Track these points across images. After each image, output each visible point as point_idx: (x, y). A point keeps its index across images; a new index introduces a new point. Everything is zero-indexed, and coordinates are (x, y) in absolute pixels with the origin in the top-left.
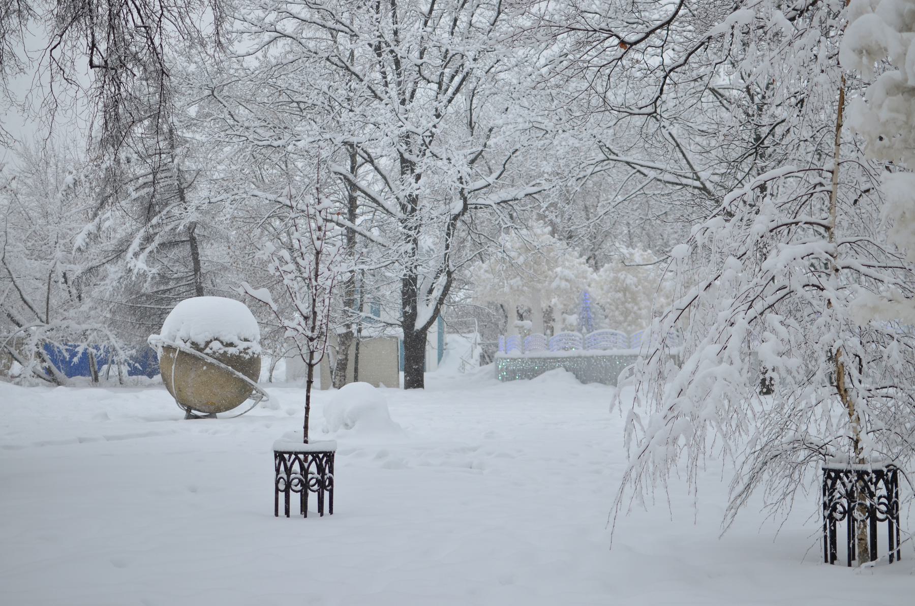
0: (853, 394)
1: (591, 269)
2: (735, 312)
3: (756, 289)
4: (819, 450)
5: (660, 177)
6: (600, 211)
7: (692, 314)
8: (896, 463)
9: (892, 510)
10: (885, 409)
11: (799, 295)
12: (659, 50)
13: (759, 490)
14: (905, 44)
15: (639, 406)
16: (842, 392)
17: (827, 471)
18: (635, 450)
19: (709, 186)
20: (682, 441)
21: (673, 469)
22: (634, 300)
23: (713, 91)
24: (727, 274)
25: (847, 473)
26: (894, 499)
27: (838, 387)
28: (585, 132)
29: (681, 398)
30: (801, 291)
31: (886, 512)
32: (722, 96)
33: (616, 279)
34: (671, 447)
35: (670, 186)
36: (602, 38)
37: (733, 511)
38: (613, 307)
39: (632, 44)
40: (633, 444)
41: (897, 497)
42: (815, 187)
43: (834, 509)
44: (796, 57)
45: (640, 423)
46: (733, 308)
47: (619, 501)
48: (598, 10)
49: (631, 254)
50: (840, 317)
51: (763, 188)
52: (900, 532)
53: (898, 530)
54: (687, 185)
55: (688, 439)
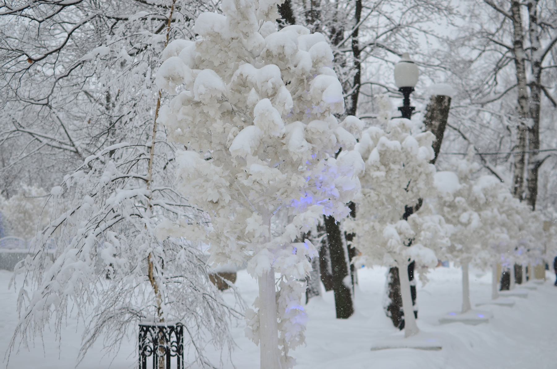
0: (157, 280)
1: (4, 198)
2: (88, 229)
3: (101, 216)
4: (137, 314)
5: (50, 143)
6: (12, 163)
7: (62, 230)
8: (183, 322)
9: (180, 349)
10: (176, 290)
11: (127, 220)
12: (53, 65)
13: (100, 338)
14: (194, 76)
15: (27, 285)
16: (151, 278)
17: (142, 327)
18: (24, 313)
19: (80, 150)
20: (53, 307)
21: (47, 326)
22: (30, 218)
23: (86, 93)
24: (85, 206)
25: (153, 328)
26: (180, 344)
27: (149, 276)
28: (4, 113)
29: (53, 281)
30: (128, 218)
31: (176, 351)
32: (92, 97)
33: (20, 205)
34: (46, 312)
35: (56, 149)
36: (17, 56)
37: (84, 351)
38: (17, 223)
39: (36, 61)
40: (23, 309)
41: (182, 342)
42: (140, 156)
43: (145, 349)
44: (134, 77)
45: (27, 296)
46: (87, 227)
47: (12, 344)
48: (17, 37)
49: (30, 190)
50: (151, 234)
51: (112, 152)
52: (184, 364)
53: (183, 362)
54: (67, 149)
55: (56, 307)
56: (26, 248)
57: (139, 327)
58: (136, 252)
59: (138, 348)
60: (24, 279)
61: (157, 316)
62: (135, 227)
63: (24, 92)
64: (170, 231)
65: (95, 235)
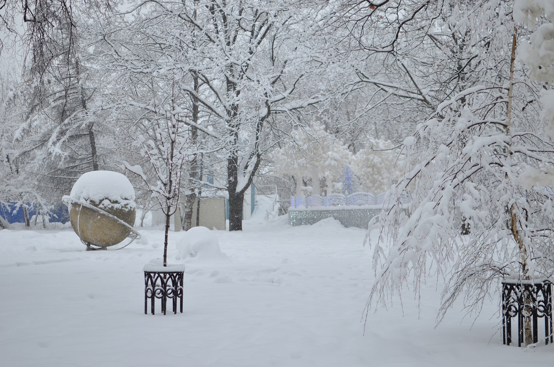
0: (522, 234)
3: (458, 166)
4: (500, 271)
5: (396, 93)
6: (357, 115)
7: (417, 182)
9: (547, 309)
10: (542, 244)
11: (486, 170)
12: (395, 10)
13: (460, 297)
16: (515, 233)
17: (505, 285)
18: (380, 271)
19: (428, 98)
20: (410, 265)
21: (404, 283)
22: (379, 173)
23: (430, 36)
25: (518, 286)
27: (512, 230)
29: (409, 237)
30: (488, 167)
31: (544, 311)
32: (436, 40)
33: (368, 159)
34: (403, 269)
35: (402, 98)
37: (444, 310)
38: (365, 178)
41: (550, 301)
42: (497, 99)
43: (510, 309)
46: (444, 178)
47: (369, 304)
50: (513, 184)
53: (551, 323)
54: (414, 98)
55: (414, 264)
56: (376, 204)
57: (502, 285)
58: (498, 203)
59: (502, 308)
60: (379, 235)
61: (522, 274)
62: (495, 176)
63: (367, 41)
64: (536, 179)
65: (452, 187)
